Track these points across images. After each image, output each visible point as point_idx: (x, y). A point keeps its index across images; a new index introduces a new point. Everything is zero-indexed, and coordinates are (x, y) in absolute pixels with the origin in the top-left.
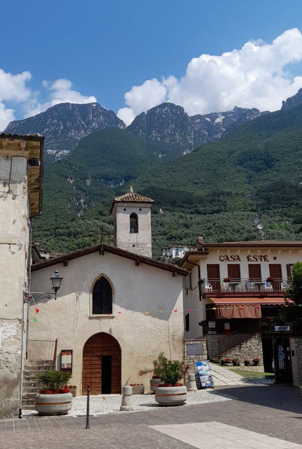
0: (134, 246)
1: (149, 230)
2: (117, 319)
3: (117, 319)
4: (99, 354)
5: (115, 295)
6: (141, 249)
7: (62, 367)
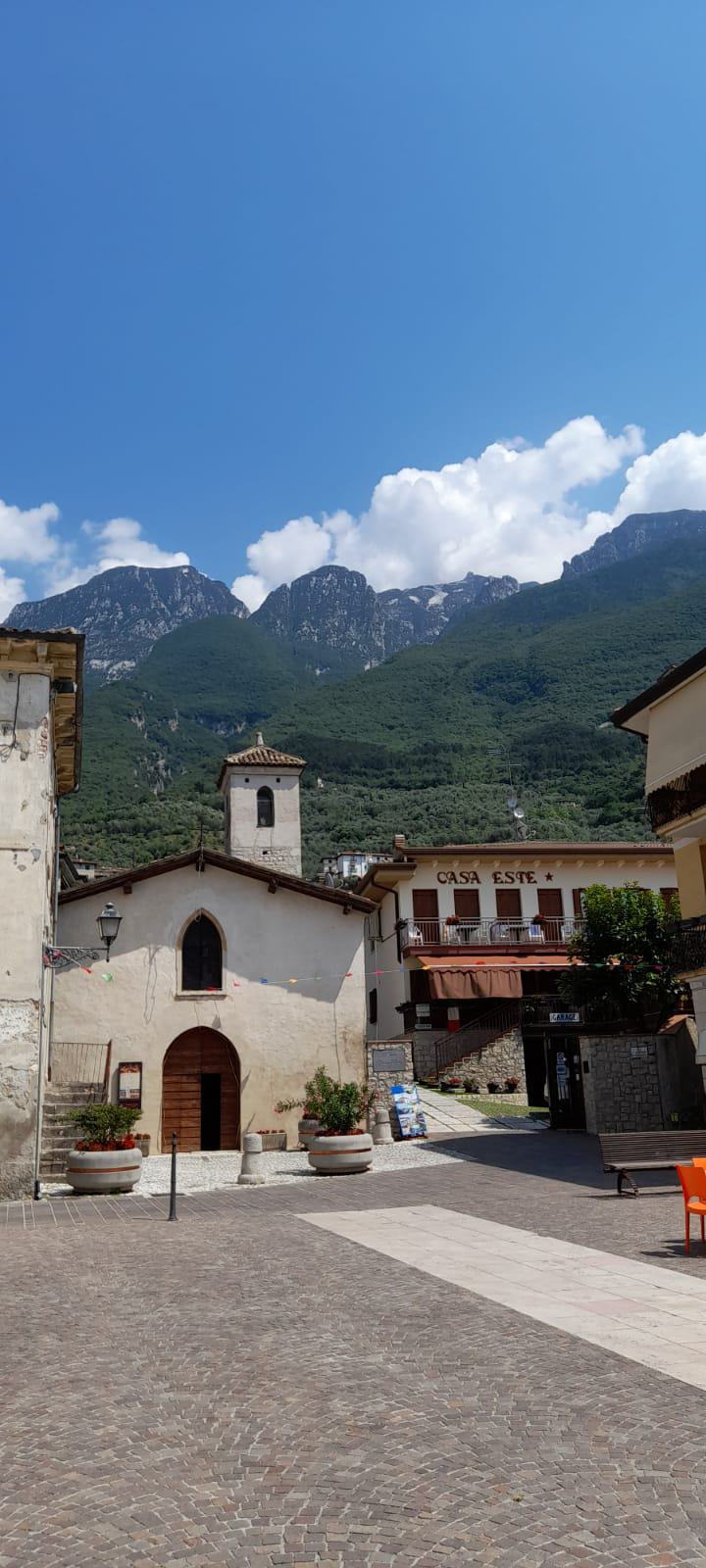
0: (265, 853)
1: (296, 820)
2: (231, 999)
3: (231, 999)
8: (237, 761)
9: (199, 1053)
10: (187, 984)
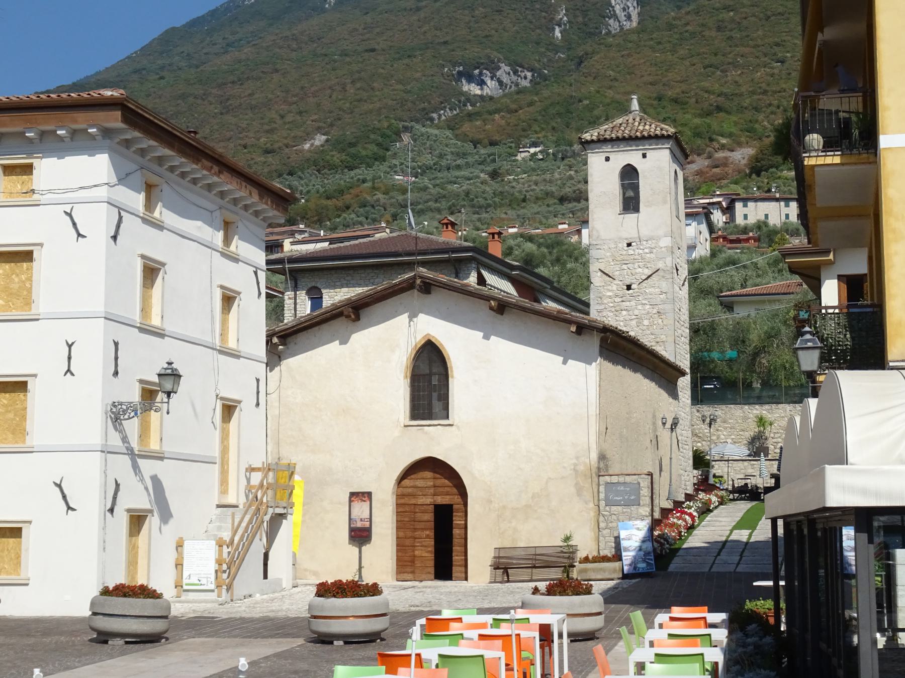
0: (629, 245)
1: (665, 202)
2: (458, 428)
3: (458, 428)
4: (429, 500)
5: (455, 380)
6: (647, 251)
7: (352, 526)
8: (594, 138)
9: (432, 483)
10: (414, 417)
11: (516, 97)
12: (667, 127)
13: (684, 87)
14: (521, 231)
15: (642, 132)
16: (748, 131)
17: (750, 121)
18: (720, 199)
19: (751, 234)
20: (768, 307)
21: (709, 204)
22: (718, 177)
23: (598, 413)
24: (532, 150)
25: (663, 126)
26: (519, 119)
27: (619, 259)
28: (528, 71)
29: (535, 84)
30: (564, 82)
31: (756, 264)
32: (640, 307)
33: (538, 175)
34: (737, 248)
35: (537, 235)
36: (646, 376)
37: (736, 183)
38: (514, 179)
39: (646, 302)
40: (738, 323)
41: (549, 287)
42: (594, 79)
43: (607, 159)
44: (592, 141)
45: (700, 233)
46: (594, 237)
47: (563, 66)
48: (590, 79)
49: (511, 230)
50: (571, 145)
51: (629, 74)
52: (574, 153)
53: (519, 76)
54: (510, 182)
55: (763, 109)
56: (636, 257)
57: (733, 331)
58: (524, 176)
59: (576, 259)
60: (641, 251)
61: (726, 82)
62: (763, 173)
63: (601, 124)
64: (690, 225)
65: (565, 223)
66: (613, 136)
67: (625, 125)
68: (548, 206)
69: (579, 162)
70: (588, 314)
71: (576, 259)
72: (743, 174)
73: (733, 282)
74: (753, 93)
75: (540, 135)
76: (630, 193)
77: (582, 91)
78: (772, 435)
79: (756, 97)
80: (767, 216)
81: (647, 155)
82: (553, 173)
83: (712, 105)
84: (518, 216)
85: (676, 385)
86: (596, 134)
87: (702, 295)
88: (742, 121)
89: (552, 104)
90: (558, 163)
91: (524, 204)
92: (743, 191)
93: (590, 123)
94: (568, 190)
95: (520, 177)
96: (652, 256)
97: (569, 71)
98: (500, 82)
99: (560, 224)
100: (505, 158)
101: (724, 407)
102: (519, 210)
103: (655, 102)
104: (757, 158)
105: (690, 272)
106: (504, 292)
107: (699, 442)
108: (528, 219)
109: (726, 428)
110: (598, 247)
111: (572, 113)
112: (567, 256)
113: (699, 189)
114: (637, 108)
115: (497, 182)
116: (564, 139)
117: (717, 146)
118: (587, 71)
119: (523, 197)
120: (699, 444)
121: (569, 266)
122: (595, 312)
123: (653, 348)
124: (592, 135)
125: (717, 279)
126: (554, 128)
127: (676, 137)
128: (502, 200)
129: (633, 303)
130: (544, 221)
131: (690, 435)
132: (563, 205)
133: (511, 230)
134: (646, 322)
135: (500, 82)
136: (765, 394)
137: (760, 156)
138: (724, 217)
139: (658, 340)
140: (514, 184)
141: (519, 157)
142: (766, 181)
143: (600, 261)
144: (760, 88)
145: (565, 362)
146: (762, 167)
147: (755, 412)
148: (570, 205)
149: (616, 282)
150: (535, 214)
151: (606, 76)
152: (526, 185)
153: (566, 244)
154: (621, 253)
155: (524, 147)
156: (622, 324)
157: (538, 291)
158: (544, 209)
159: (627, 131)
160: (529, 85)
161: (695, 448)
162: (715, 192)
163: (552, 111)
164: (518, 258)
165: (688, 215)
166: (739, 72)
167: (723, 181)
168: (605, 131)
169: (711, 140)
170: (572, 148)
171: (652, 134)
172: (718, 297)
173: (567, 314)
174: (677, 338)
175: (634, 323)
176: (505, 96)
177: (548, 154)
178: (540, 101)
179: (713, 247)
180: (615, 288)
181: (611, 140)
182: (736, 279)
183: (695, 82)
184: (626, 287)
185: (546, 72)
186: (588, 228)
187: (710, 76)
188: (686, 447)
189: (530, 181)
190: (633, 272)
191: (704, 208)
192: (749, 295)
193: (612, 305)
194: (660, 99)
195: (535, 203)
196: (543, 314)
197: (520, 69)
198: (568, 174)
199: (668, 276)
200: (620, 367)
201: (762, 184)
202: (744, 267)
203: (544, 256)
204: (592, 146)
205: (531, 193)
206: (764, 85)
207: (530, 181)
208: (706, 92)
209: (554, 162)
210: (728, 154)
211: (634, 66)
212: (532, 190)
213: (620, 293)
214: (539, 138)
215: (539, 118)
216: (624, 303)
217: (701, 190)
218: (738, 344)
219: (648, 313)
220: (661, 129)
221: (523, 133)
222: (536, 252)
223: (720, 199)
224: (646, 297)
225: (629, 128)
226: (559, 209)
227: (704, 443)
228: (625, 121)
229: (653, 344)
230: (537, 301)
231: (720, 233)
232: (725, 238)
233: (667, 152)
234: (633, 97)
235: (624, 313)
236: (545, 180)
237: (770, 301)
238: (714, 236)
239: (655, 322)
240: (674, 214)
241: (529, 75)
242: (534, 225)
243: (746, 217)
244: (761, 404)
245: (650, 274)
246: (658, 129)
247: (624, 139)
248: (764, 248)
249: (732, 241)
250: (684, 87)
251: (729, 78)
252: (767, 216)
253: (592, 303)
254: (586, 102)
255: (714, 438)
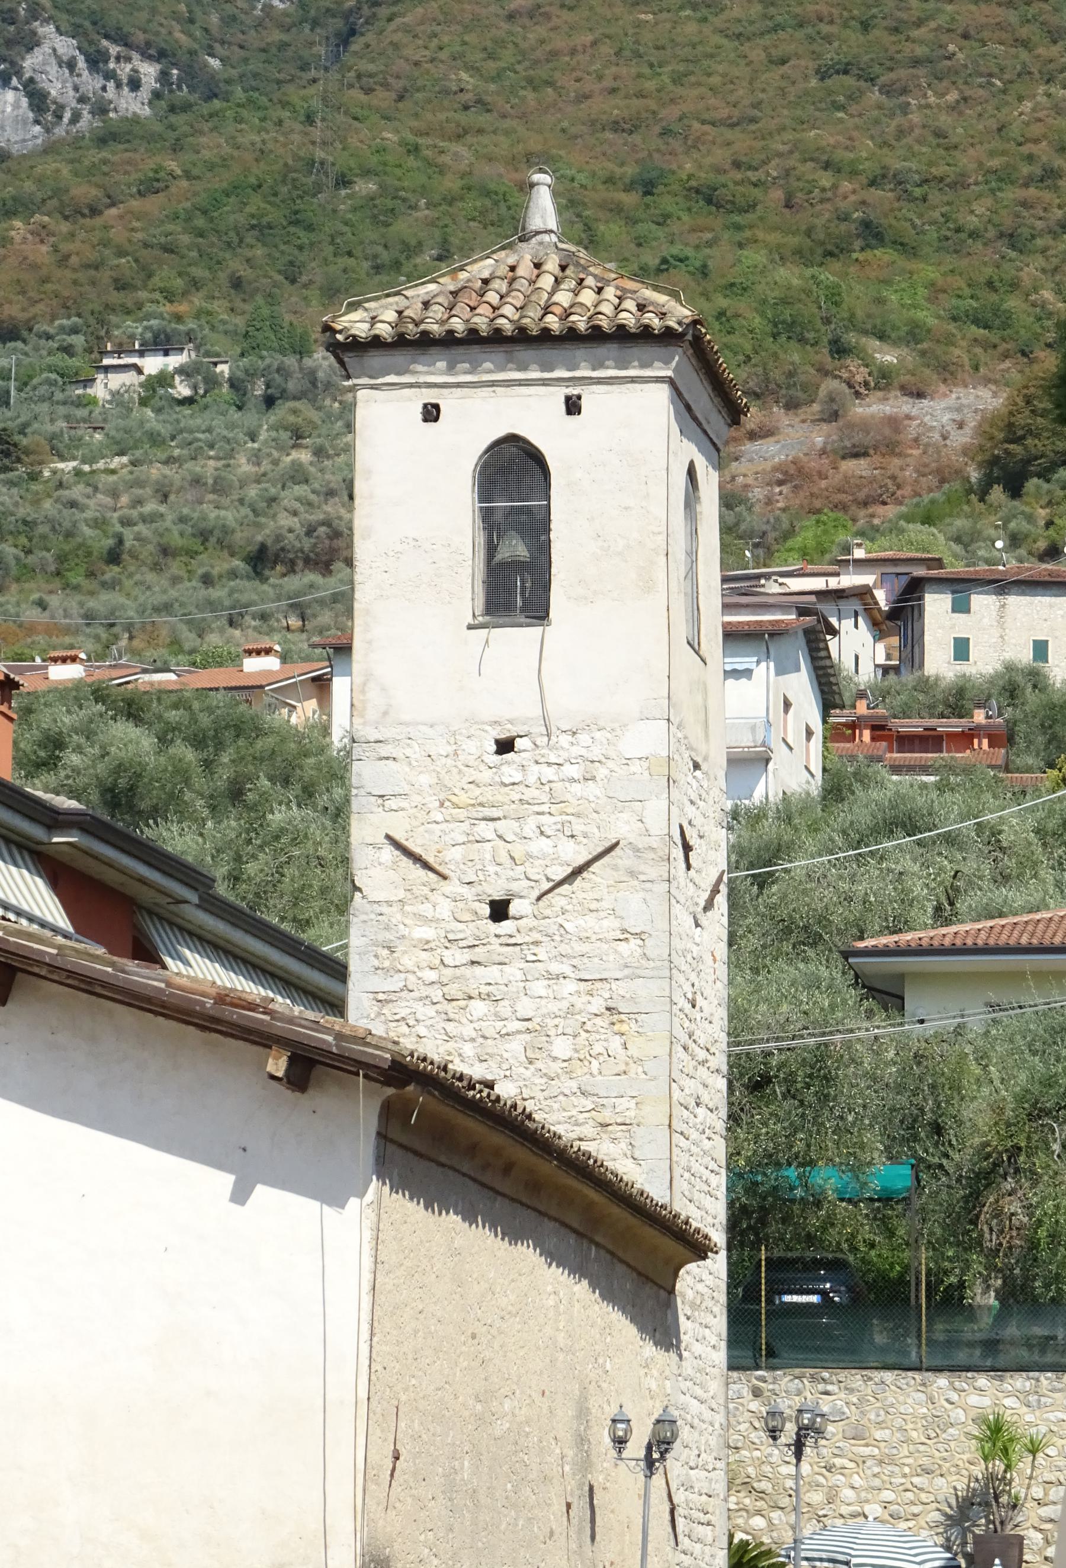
0: (505, 746)
8: (384, 330)
11: (94, 155)
12: (662, 298)
13: (742, 142)
14: (99, 675)
15: (567, 314)
16: (976, 322)
17: (990, 284)
18: (867, 579)
19: (979, 717)
20: (1035, 999)
21: (823, 595)
22: (862, 495)
23: (363, 1395)
24: (153, 364)
25: (648, 294)
26: (105, 243)
27: (463, 798)
28: (147, 57)
29: (172, 109)
30: (285, 104)
31: (996, 833)
32: (539, 987)
33: (168, 461)
34: (925, 769)
35: (161, 693)
36: (553, 1256)
37: (928, 520)
38: (78, 473)
39: (567, 970)
40: (918, 1058)
41: (194, 898)
42: (401, 98)
43: (431, 413)
44: (376, 342)
45: (787, 705)
46: (372, 714)
47: (283, 46)
48: (383, 98)
49: (62, 673)
50: (302, 351)
51: (532, 83)
52: (314, 383)
53: (110, 75)
54: (60, 485)
55: (1039, 242)
56: (530, 794)
57: (900, 1089)
58: (116, 462)
59: (308, 793)
60: (549, 773)
61: (901, 133)
62: (1032, 484)
63: (416, 276)
64: (747, 673)
65: (268, 651)
66: (457, 325)
67: (503, 287)
68: (207, 580)
69: (329, 418)
70: (336, 1006)
71: (308, 793)
72: (957, 485)
73: (907, 901)
74: (1004, 177)
75: (182, 308)
76: (515, 548)
77: (353, 141)
78: (1037, 1492)
79: (1011, 194)
80: (1041, 649)
81: (584, 403)
82: (230, 455)
83: (845, 218)
84: (89, 617)
85: (671, 1291)
86: (391, 316)
87: (787, 947)
88: (961, 283)
89: (234, 189)
90: (249, 418)
91: (112, 572)
92: (958, 549)
93: (378, 269)
94: (285, 521)
95: (101, 465)
96: (592, 790)
97: (304, 67)
98: (38, 99)
99: (249, 653)
100: (43, 390)
101: (855, 1378)
102: (92, 593)
103: (630, 199)
104: (1010, 425)
105: (739, 855)
106: (31, 919)
107: (759, 1512)
108: (129, 628)
109: (860, 1462)
110: (384, 750)
111: (310, 228)
112: (271, 779)
113: (789, 534)
114: (552, 224)
115: (11, 484)
116: (275, 328)
117: (861, 375)
118: (371, 68)
119: (110, 542)
120: (758, 1522)
121: (277, 817)
122: (367, 1001)
123: (585, 1146)
124: (374, 320)
125: (844, 886)
126: (237, 284)
127: (698, 339)
128: (28, 552)
129: (513, 971)
130: (189, 639)
131: (720, 1487)
132: (264, 580)
133: (62, 673)
134: (562, 1047)
135: (38, 99)
136: (1012, 1331)
137: (1022, 419)
138: (881, 648)
139: (606, 1116)
140: (77, 492)
141: (101, 389)
142: (1043, 513)
143: (392, 803)
144: (1030, 158)
145: (240, 1195)
146: (1028, 462)
147: (974, 1399)
148: (294, 582)
149: (452, 887)
150: (157, 610)
151: (446, 92)
152: (124, 500)
153: (272, 731)
154: (472, 774)
155: (119, 352)
156: (468, 1049)
157: (150, 913)
158: (190, 591)
159: (508, 310)
160: (147, 111)
161: (739, 1536)
162: (847, 549)
163: (232, 216)
164: (82, 781)
165: (733, 636)
166: (952, 97)
167: (880, 510)
168: (426, 305)
169: (840, 350)
170: (308, 362)
171: (604, 323)
172: (846, 955)
173: (252, 1006)
174: (678, 1111)
175: (515, 1047)
176: (49, 149)
177: (212, 382)
178: (188, 175)
179: (835, 763)
180: (445, 909)
181: (449, 341)
182: (918, 890)
183: (782, 129)
184: (486, 910)
185: (214, 63)
186: (350, 674)
187: (842, 108)
188: (705, 1532)
189: (139, 483)
190: (518, 849)
191: (802, 612)
192: (976, 951)
193: (432, 976)
194: (648, 187)
195: (156, 567)
196: (149, 1000)
197: (114, 50)
198: (289, 459)
199: (654, 872)
200: (453, 1220)
201: (1025, 526)
202: (950, 839)
203: (183, 774)
204: (376, 359)
205: (140, 528)
206: (1043, 150)
207: (139, 483)
208: (827, 166)
209: (235, 415)
210: (904, 406)
211: (554, 54)
212: (148, 519)
213: (467, 932)
214: (178, 318)
215: (185, 239)
216: (478, 970)
217: (796, 542)
218: (916, 1138)
219: (571, 1011)
220: (641, 307)
221: (115, 297)
222: (151, 760)
223: (867, 579)
224: (564, 948)
225: (517, 299)
226: (244, 598)
227: (775, 1515)
228: (503, 270)
229: (588, 1131)
230: (147, 954)
231: (862, 708)
232: (879, 729)
233: (663, 392)
234: (537, 177)
235: (479, 1008)
236: (197, 481)
237: (1041, 976)
238: (838, 717)
239: (598, 1048)
240: (681, 631)
241: (149, 71)
242: (150, 654)
243: (961, 649)
244: (998, 1369)
245: (581, 860)
246: (630, 304)
247: (497, 339)
248: (1029, 770)
249: (906, 742)
250: (742, 142)
251: (915, 118)
252: (1041, 649)
253: (355, 966)
254: (366, 187)
255: (816, 1497)
